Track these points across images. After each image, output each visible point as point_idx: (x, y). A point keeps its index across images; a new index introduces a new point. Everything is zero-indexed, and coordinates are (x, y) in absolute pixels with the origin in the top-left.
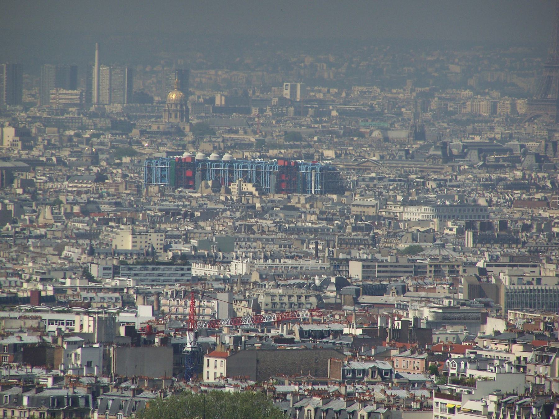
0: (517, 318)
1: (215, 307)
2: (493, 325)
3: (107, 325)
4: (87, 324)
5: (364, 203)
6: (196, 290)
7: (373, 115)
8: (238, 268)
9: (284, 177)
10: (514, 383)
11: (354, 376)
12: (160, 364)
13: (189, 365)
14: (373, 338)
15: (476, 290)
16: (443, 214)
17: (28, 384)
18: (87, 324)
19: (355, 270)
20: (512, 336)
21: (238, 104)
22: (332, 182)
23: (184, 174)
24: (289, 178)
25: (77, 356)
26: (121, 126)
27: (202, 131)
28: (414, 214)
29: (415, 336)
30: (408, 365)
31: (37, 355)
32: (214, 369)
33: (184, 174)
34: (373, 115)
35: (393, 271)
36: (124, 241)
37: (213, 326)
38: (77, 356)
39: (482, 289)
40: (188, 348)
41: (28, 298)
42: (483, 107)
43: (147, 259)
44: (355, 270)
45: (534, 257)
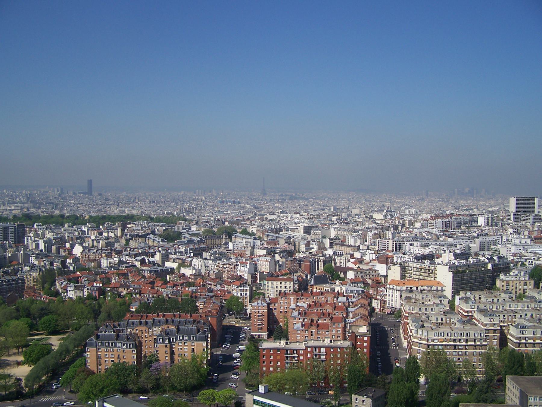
0: (259, 217)
1: (226, 216)
2: (257, 218)
3: (215, 219)
4: (213, 219)
5: (242, 205)
6: (225, 215)
7: (244, 195)
8: (229, 212)
9: (473, 281)
10: (259, 224)
11: (242, 224)
12: (220, 223)
13: (224, 223)
14: (244, 219)
15: (255, 214)
16: (251, 206)
17: (206, 225)
18: (213, 219)
19: (242, 212)
20: (259, 219)
21: (229, 194)
22: (239, 203)
23: (223, 202)
24: (234, 202)
25: (212, 222)
26: (216, 197)
27: (225, 197)
28: (248, 206)
29: (248, 219)
30: (248, 222)
31: (207, 222)
32: (226, 223)
33: (223, 202)
34: (244, 195)
35: (246, 212)
36: (217, 209)
37: (227, 219)
38: (212, 222)
39: (255, 214)
40: (55, 348)
41: (59, 253)
42: (255, 194)
43: (219, 211)
44: (242, 212)
45: (261, 211)
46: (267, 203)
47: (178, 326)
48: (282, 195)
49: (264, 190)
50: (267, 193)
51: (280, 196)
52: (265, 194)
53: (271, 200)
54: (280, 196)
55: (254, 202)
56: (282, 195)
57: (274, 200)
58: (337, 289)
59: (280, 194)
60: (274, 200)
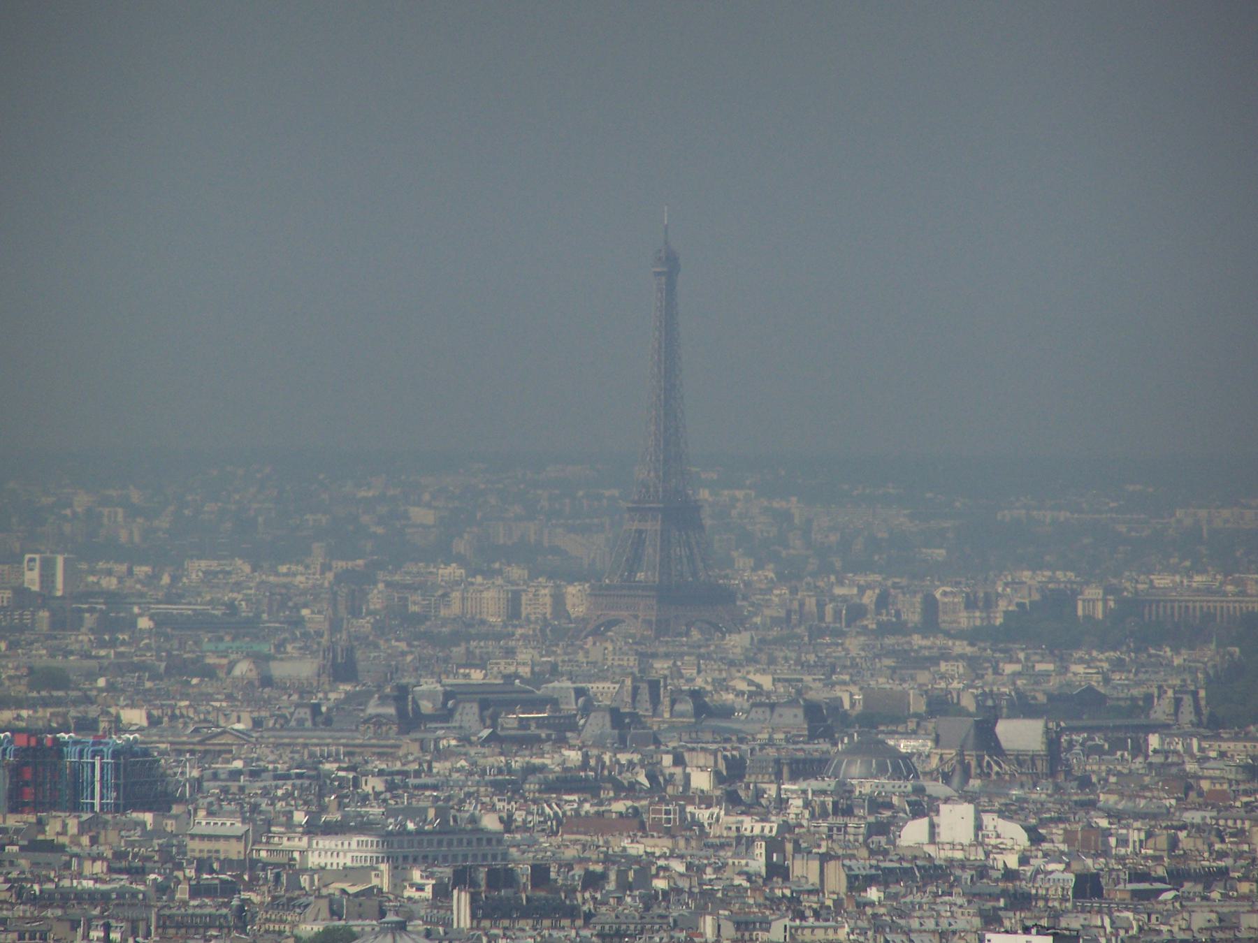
5: (216, 830)
7: (234, 624)
16: (401, 851)
22: (141, 782)
28: (333, 854)
34: (234, 624)
42: (489, 602)
46: (733, 787)
47: (732, 663)
48: (1048, 624)
49: (681, 515)
50: (744, 572)
51: (1018, 631)
52: (695, 601)
53: (822, 719)
54: (1018, 631)
55: (458, 761)
56: (1048, 624)
57: (882, 716)
58: (778, 893)
59: (1018, 588)
60: (882, 716)
